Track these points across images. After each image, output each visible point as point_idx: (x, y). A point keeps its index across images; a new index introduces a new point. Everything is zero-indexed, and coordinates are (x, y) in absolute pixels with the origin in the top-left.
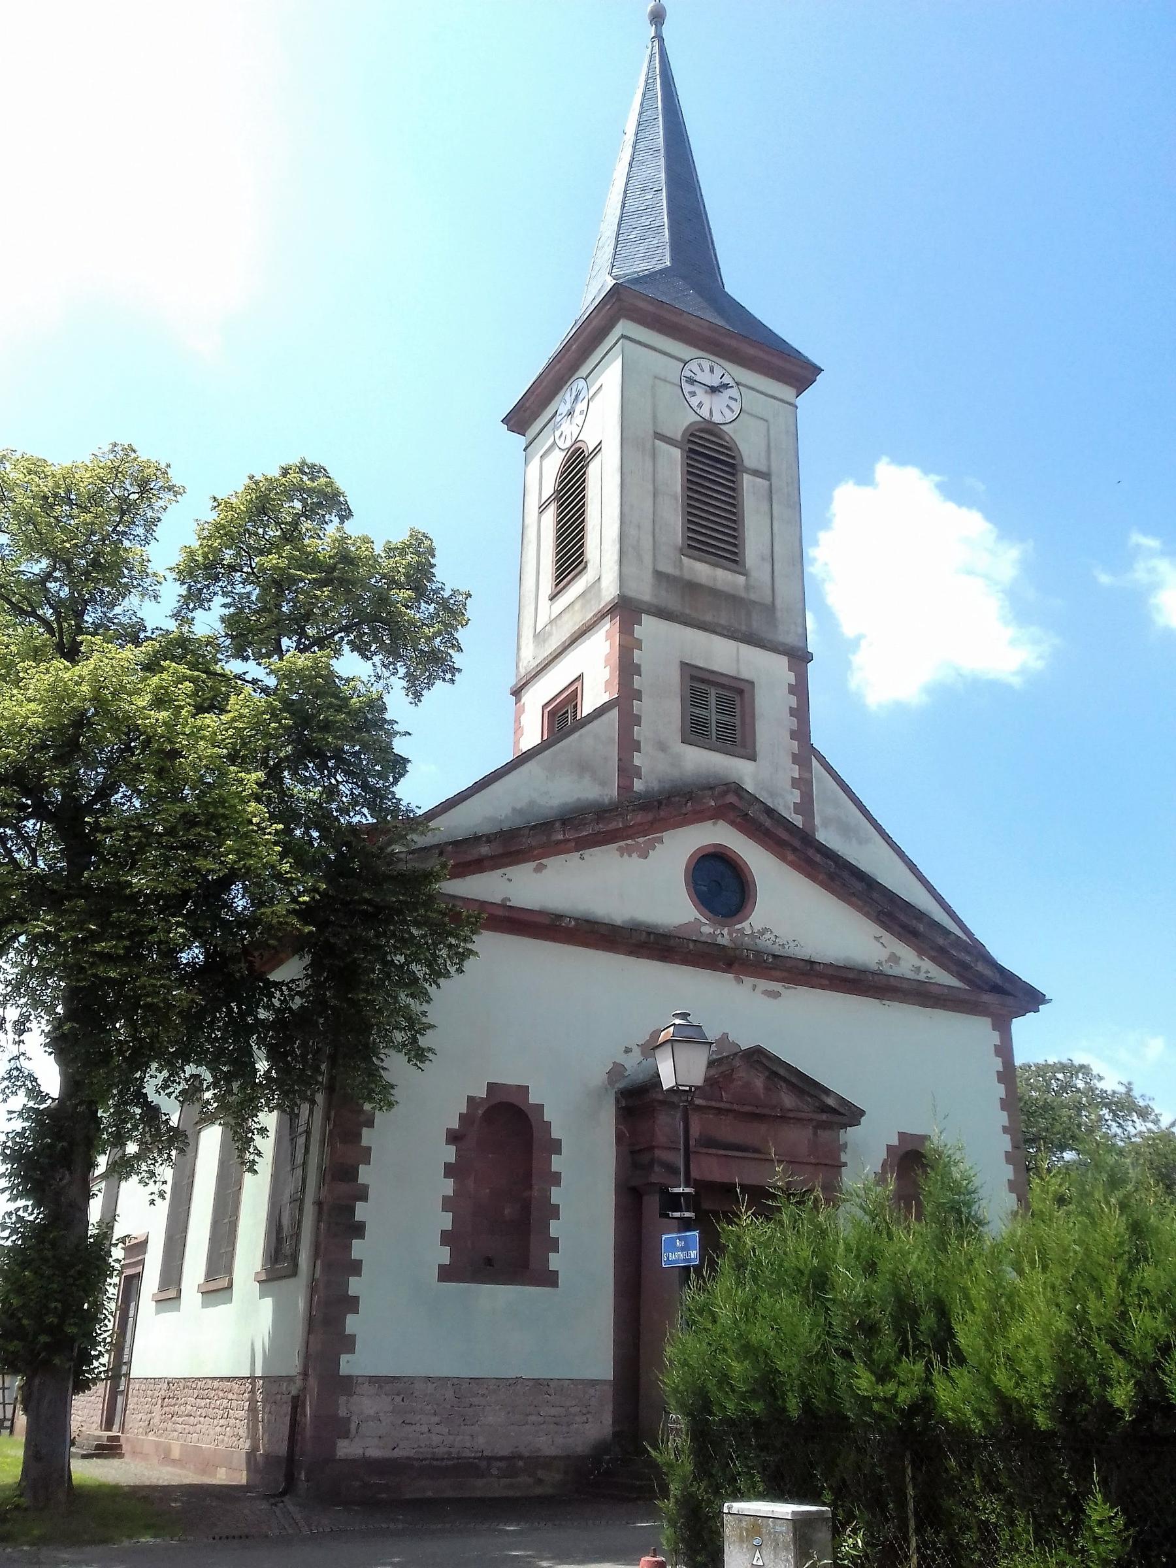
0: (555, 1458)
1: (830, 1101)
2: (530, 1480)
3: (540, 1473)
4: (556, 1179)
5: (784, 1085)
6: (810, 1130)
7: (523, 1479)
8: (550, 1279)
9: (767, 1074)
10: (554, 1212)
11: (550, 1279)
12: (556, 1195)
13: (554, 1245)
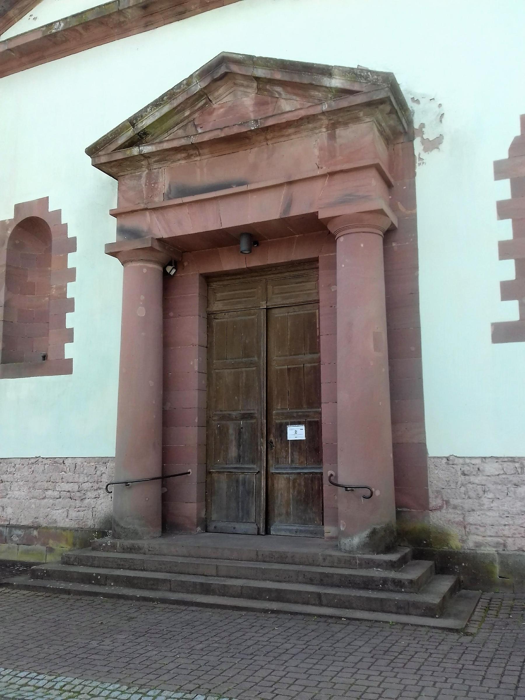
0: (64, 529)
1: (336, 82)
2: (44, 548)
3: (51, 543)
4: (71, 275)
5: (279, 89)
6: (323, 135)
7: (38, 547)
8: (65, 367)
9: (255, 85)
10: (70, 305)
11: (65, 367)
12: (72, 290)
13: (69, 336)
